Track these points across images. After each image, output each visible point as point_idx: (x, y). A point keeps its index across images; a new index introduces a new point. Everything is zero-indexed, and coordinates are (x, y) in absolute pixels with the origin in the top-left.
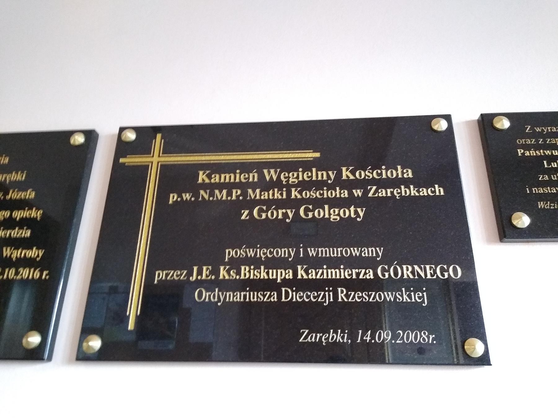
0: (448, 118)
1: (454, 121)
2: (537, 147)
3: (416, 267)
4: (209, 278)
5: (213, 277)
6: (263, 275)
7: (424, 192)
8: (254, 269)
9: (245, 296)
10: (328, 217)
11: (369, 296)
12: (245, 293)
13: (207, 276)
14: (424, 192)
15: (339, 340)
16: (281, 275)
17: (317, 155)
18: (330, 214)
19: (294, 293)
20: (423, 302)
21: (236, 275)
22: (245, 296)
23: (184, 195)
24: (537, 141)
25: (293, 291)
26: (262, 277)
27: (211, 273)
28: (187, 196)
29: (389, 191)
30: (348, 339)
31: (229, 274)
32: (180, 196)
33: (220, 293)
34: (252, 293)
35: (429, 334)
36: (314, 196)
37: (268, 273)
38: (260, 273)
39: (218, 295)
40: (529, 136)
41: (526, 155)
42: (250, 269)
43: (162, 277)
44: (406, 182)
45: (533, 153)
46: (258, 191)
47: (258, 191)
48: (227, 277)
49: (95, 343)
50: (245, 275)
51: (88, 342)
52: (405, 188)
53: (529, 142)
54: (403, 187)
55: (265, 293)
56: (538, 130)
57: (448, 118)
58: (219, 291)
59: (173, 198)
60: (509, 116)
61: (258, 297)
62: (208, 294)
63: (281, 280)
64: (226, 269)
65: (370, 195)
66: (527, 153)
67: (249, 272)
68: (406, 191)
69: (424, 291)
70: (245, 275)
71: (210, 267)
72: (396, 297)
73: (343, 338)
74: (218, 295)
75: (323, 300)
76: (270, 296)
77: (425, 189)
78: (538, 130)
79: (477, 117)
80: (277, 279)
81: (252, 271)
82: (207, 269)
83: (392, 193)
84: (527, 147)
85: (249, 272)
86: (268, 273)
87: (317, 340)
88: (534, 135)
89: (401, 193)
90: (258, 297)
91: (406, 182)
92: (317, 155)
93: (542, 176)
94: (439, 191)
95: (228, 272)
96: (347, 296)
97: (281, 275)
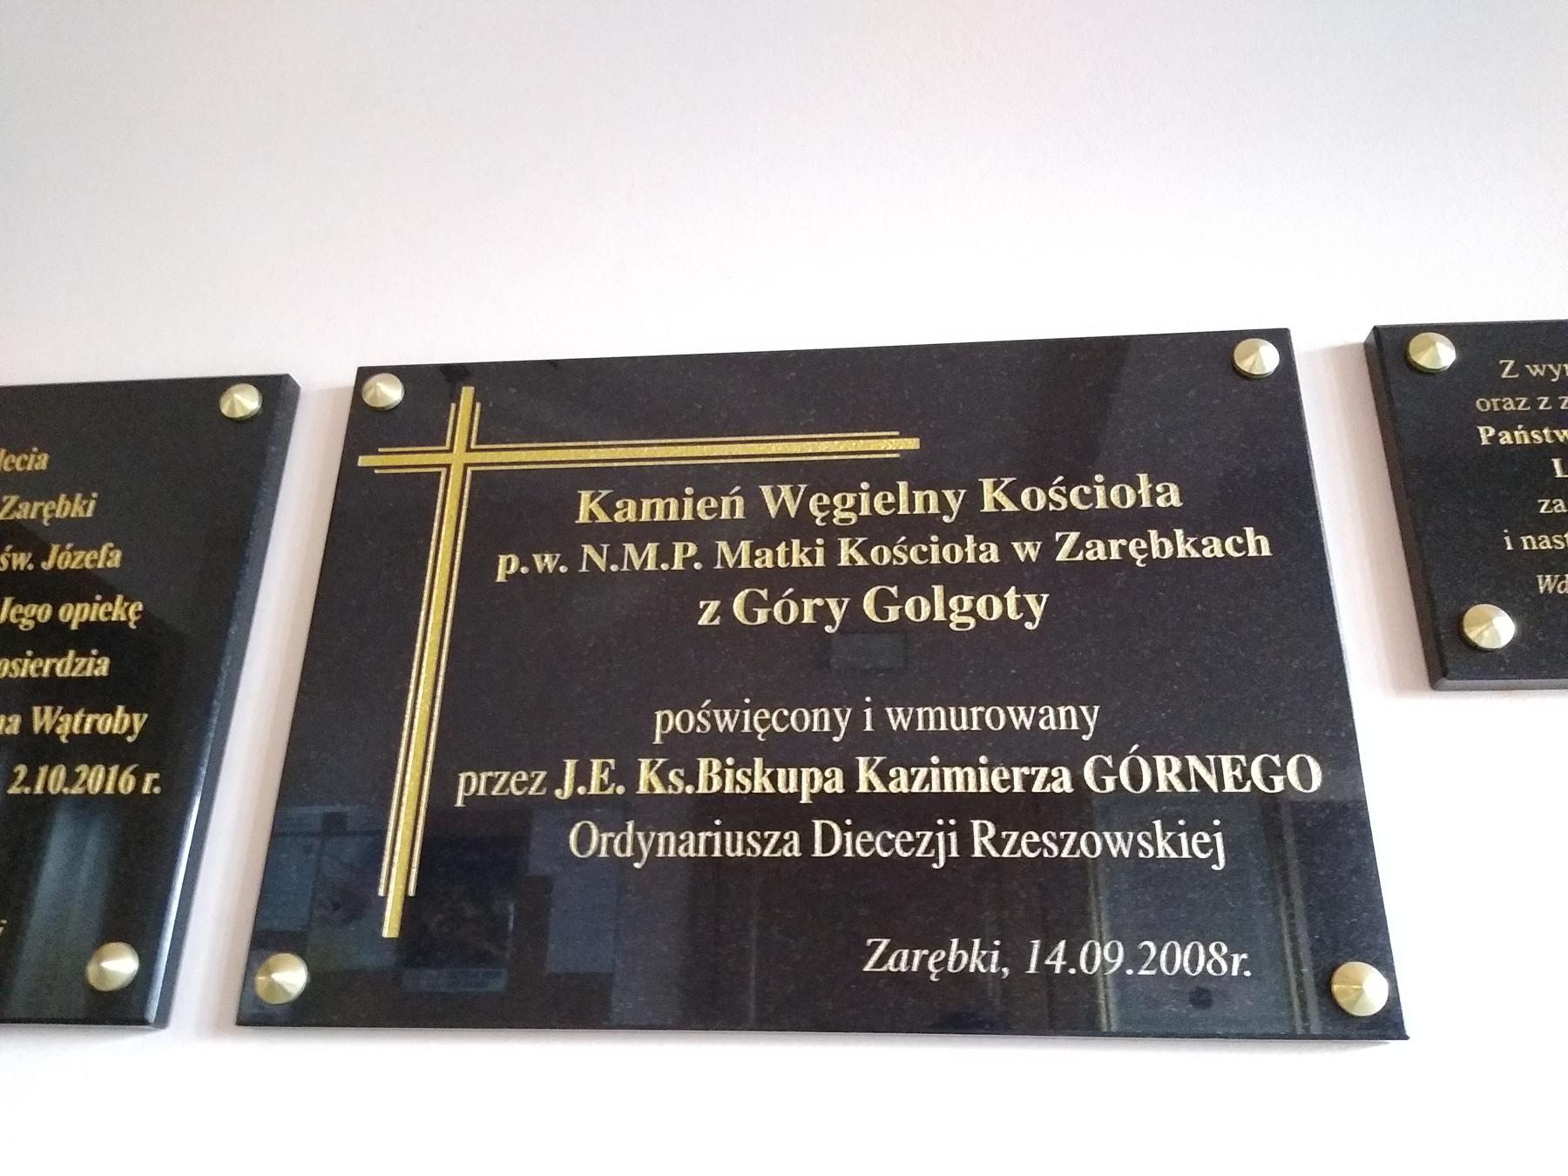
2: (1533, 421)
3: (1193, 761)
6: (761, 784)
7: (1214, 548)
8: (735, 768)
9: (710, 843)
13: (603, 787)
14: (1214, 548)
22: (710, 843)
24: (1533, 403)
25: (844, 829)
27: (615, 777)
28: (546, 562)
30: (1001, 964)
31: (666, 782)
32: (526, 560)
33: (640, 835)
34: (729, 835)
35: (1232, 950)
37: (773, 779)
40: (1513, 389)
41: (1502, 442)
42: (725, 766)
44: (1164, 521)
45: (1521, 436)
53: (1509, 405)
56: (1536, 371)
58: (636, 829)
59: (507, 566)
62: (605, 837)
63: (812, 796)
66: (1506, 438)
67: (722, 774)
69: (1217, 829)
72: (1136, 847)
73: (986, 961)
74: (635, 838)
76: (780, 843)
77: (1216, 541)
78: (1536, 371)
79: (1362, 335)
80: (798, 795)
81: (729, 772)
82: (604, 766)
83: (1123, 550)
84: (1504, 421)
85: (722, 774)
86: (773, 779)
88: (1524, 386)
90: (746, 845)
91: (1164, 521)
93: (1547, 502)
94: (1257, 544)
95: (662, 774)
96: (999, 843)
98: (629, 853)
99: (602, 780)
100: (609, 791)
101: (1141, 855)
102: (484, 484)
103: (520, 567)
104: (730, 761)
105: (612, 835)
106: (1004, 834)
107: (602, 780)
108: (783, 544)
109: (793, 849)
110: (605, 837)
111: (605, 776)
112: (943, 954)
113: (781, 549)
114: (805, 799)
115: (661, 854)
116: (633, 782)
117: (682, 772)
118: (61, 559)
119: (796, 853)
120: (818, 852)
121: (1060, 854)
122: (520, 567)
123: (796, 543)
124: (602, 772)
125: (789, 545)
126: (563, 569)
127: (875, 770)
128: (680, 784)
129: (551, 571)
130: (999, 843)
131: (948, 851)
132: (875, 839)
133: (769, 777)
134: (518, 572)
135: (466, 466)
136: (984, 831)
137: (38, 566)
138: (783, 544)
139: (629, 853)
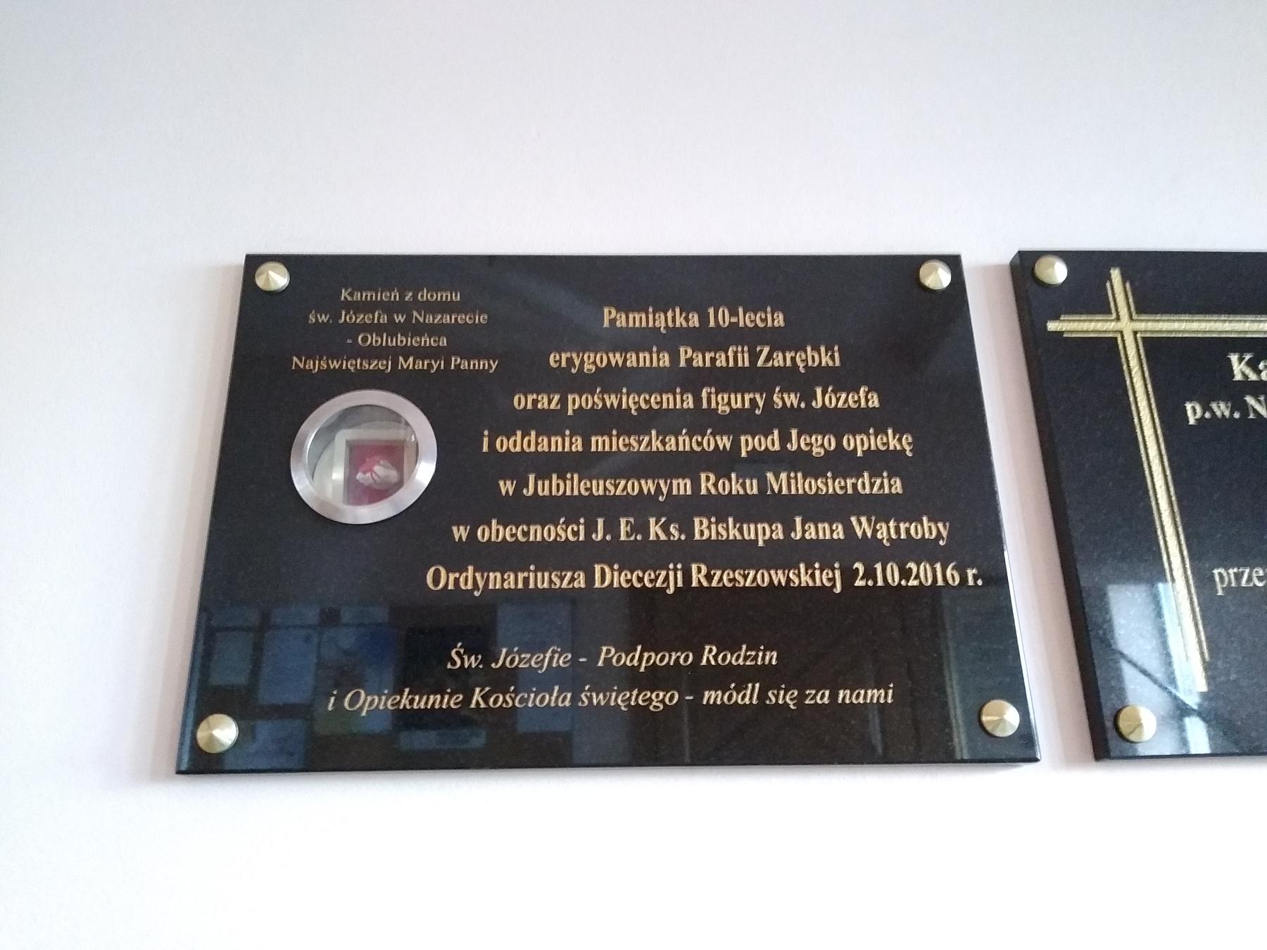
0: (953, 262)
1: (966, 263)
4: (632, 538)
5: (639, 537)
6: (734, 533)
8: (717, 523)
9: (526, 580)
10: (715, 407)
11: (745, 577)
12: (526, 574)
13: (628, 535)
15: (478, 703)
16: (764, 534)
17: (1052, 326)
18: (717, 403)
19: (616, 574)
20: (834, 586)
21: (680, 535)
22: (526, 580)
23: (1214, 406)
25: (612, 570)
26: (731, 537)
27: (634, 529)
28: (1221, 409)
29: (789, 355)
31: (668, 533)
32: (1206, 408)
33: (478, 575)
34: (539, 575)
36: (592, 370)
37: (741, 530)
38: (727, 530)
39: (475, 578)
42: (710, 523)
43: (490, 537)
46: (411, 359)
47: (411, 359)
48: (663, 537)
49: (224, 732)
50: (702, 533)
51: (210, 728)
52: (812, 350)
54: (809, 349)
55: (563, 574)
57: (953, 262)
58: (475, 571)
59: (1193, 412)
60: (1067, 256)
61: (551, 581)
62: (452, 577)
63: (765, 541)
64: (660, 524)
65: (760, 363)
67: (709, 528)
68: (813, 357)
70: (702, 533)
71: (632, 520)
72: (789, 580)
74: (475, 578)
75: (665, 585)
76: (572, 580)
80: (756, 541)
81: (713, 527)
82: (627, 522)
85: (709, 528)
86: (741, 530)
87: (429, 707)
89: (806, 360)
90: (551, 581)
92: (1052, 326)
95: (665, 528)
96: (709, 577)
97: (764, 534)
98: (470, 586)
99: (627, 531)
100: (632, 538)
101: (792, 585)
102: (1108, 348)
103: (1204, 413)
104: (713, 520)
105: (457, 575)
106: (712, 572)
107: (627, 531)
108: (670, 311)
109: (581, 583)
110: (452, 577)
111: (629, 529)
112: (542, 656)
113: (670, 314)
114: (761, 543)
115: (491, 587)
116: (646, 532)
117: (677, 526)
118: (824, 399)
119: (583, 586)
120: (597, 585)
121: (745, 584)
122: (1204, 413)
123: (678, 310)
124: (627, 526)
125: (674, 311)
126: (1237, 415)
127: (660, 526)
128: (676, 533)
129: (620, 365)
130: (709, 577)
131: (676, 583)
132: (632, 577)
133: (738, 529)
134: (1203, 417)
135: (1121, 332)
136: (699, 570)
137: (808, 405)
138: (670, 311)
139: (470, 586)
